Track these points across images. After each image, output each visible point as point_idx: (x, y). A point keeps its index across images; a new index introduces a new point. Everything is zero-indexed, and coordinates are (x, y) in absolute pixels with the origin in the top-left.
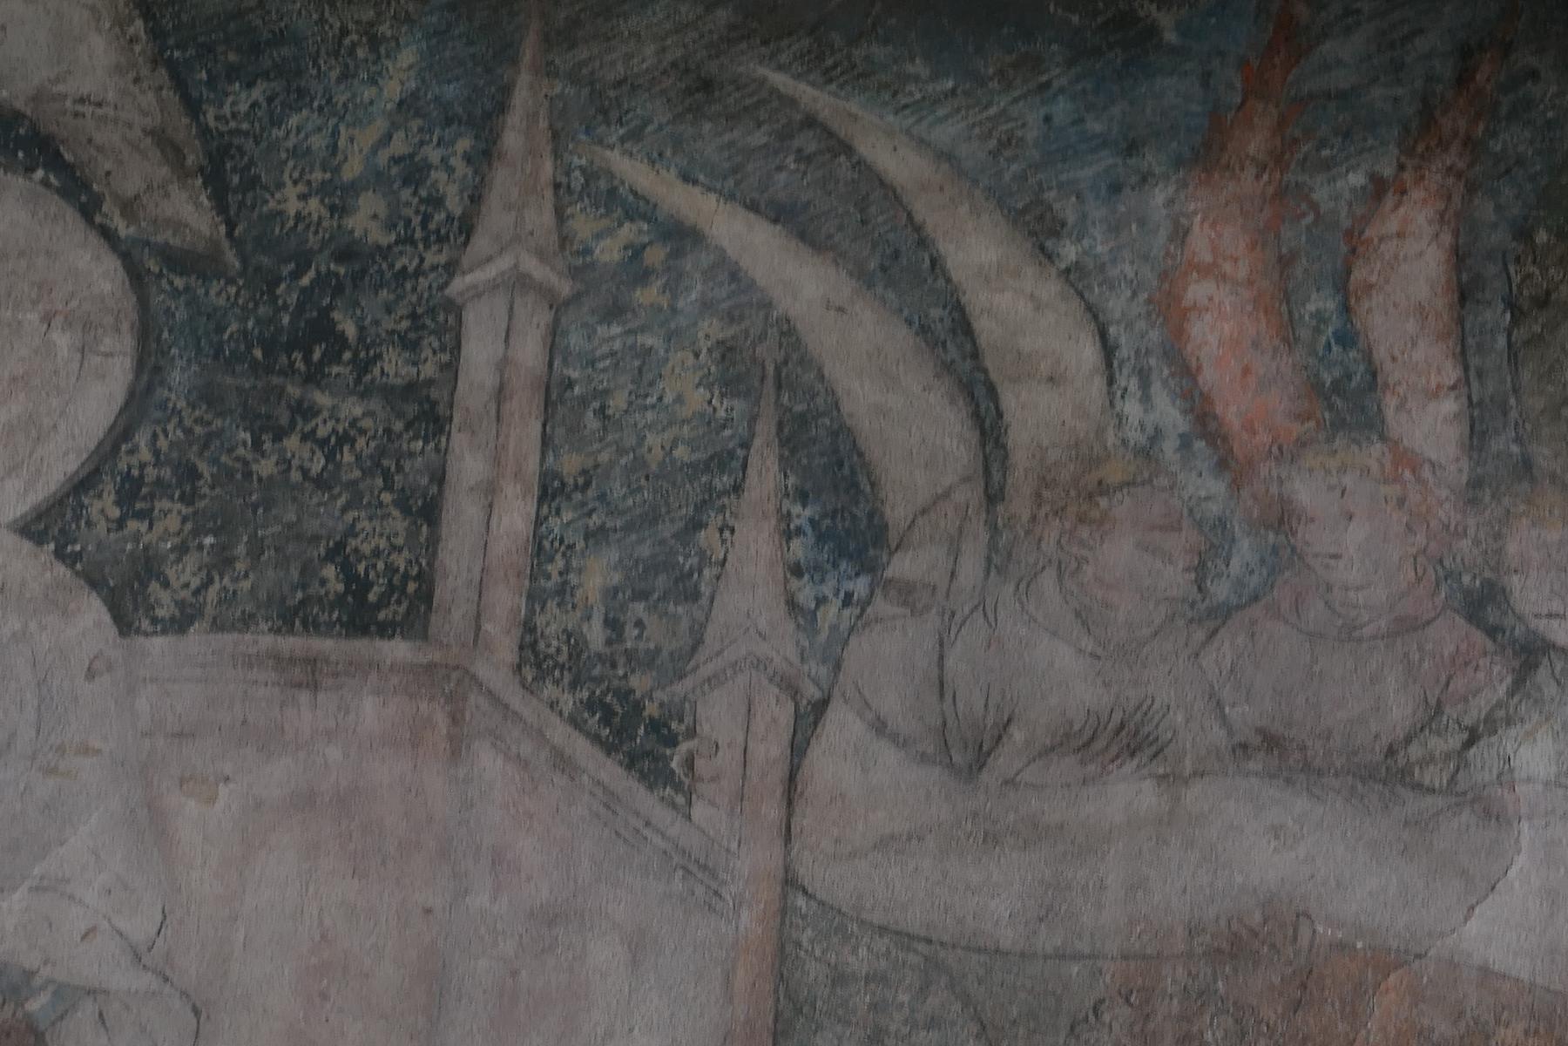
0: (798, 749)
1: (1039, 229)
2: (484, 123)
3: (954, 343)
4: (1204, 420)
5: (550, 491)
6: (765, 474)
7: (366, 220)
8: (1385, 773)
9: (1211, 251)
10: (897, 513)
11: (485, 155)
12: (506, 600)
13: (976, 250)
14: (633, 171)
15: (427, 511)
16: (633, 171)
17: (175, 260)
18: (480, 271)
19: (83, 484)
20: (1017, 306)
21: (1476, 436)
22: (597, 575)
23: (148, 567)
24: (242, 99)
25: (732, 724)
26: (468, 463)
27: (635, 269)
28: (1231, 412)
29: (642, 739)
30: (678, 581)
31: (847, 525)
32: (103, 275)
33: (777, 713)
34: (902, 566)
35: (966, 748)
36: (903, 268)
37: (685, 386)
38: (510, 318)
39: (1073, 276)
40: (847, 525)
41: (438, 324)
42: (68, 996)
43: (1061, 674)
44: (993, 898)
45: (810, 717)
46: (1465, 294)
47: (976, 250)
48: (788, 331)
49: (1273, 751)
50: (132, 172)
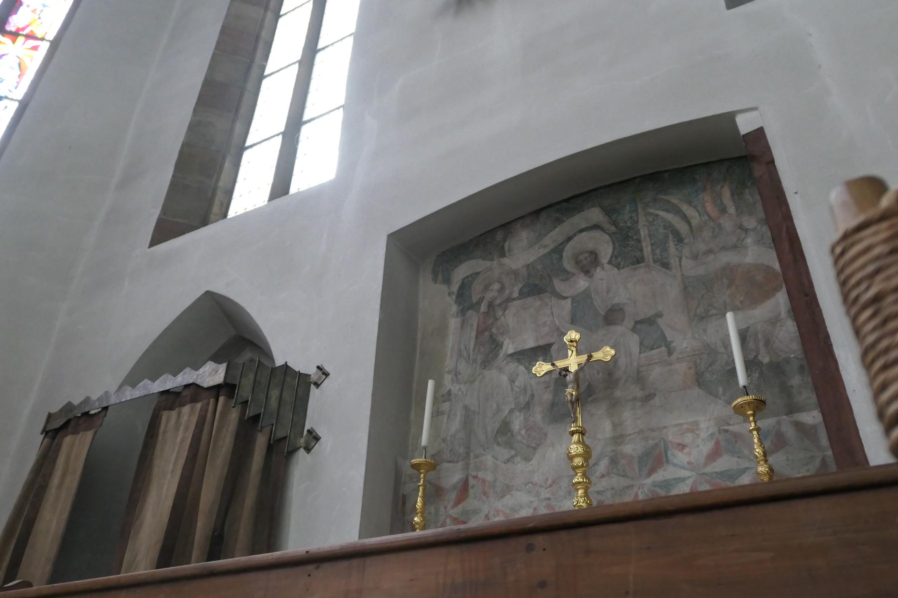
0: (680, 262)
1: (690, 203)
2: (636, 210)
3: (686, 219)
4: (710, 218)
5: (652, 245)
6: (671, 237)
7: (629, 224)
8: (735, 247)
9: (706, 198)
10: (683, 236)
11: (637, 214)
12: (651, 257)
13: (685, 208)
14: (651, 211)
15: (642, 250)
16: (651, 211)
17: (613, 234)
18: (640, 226)
19: (612, 257)
20: (689, 211)
21: (737, 209)
22: (658, 252)
23: (619, 264)
24: (614, 216)
25: (674, 262)
26: (644, 245)
27: (654, 220)
28: (712, 215)
29: (666, 266)
30: (665, 250)
31: (680, 240)
32: (607, 237)
33: (677, 259)
34: (686, 241)
35: (695, 257)
36: (678, 212)
37: (661, 230)
38: (717, 161)
39: (695, 207)
40: (680, 240)
41: (638, 232)
42: (624, 304)
43: (702, 247)
44: (701, 271)
45: (680, 259)
46: (733, 195)
47: (685, 208)
48: (669, 222)
49: (724, 248)
50: (606, 226)
